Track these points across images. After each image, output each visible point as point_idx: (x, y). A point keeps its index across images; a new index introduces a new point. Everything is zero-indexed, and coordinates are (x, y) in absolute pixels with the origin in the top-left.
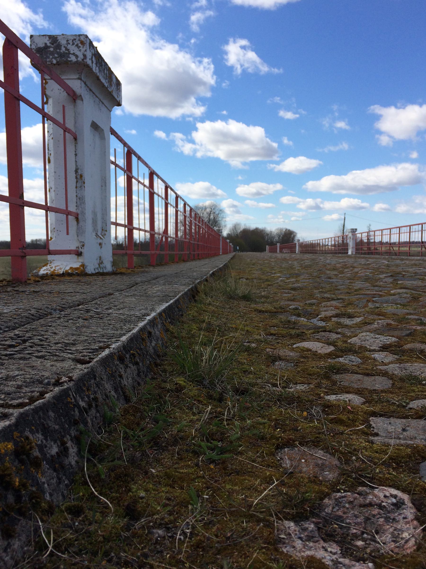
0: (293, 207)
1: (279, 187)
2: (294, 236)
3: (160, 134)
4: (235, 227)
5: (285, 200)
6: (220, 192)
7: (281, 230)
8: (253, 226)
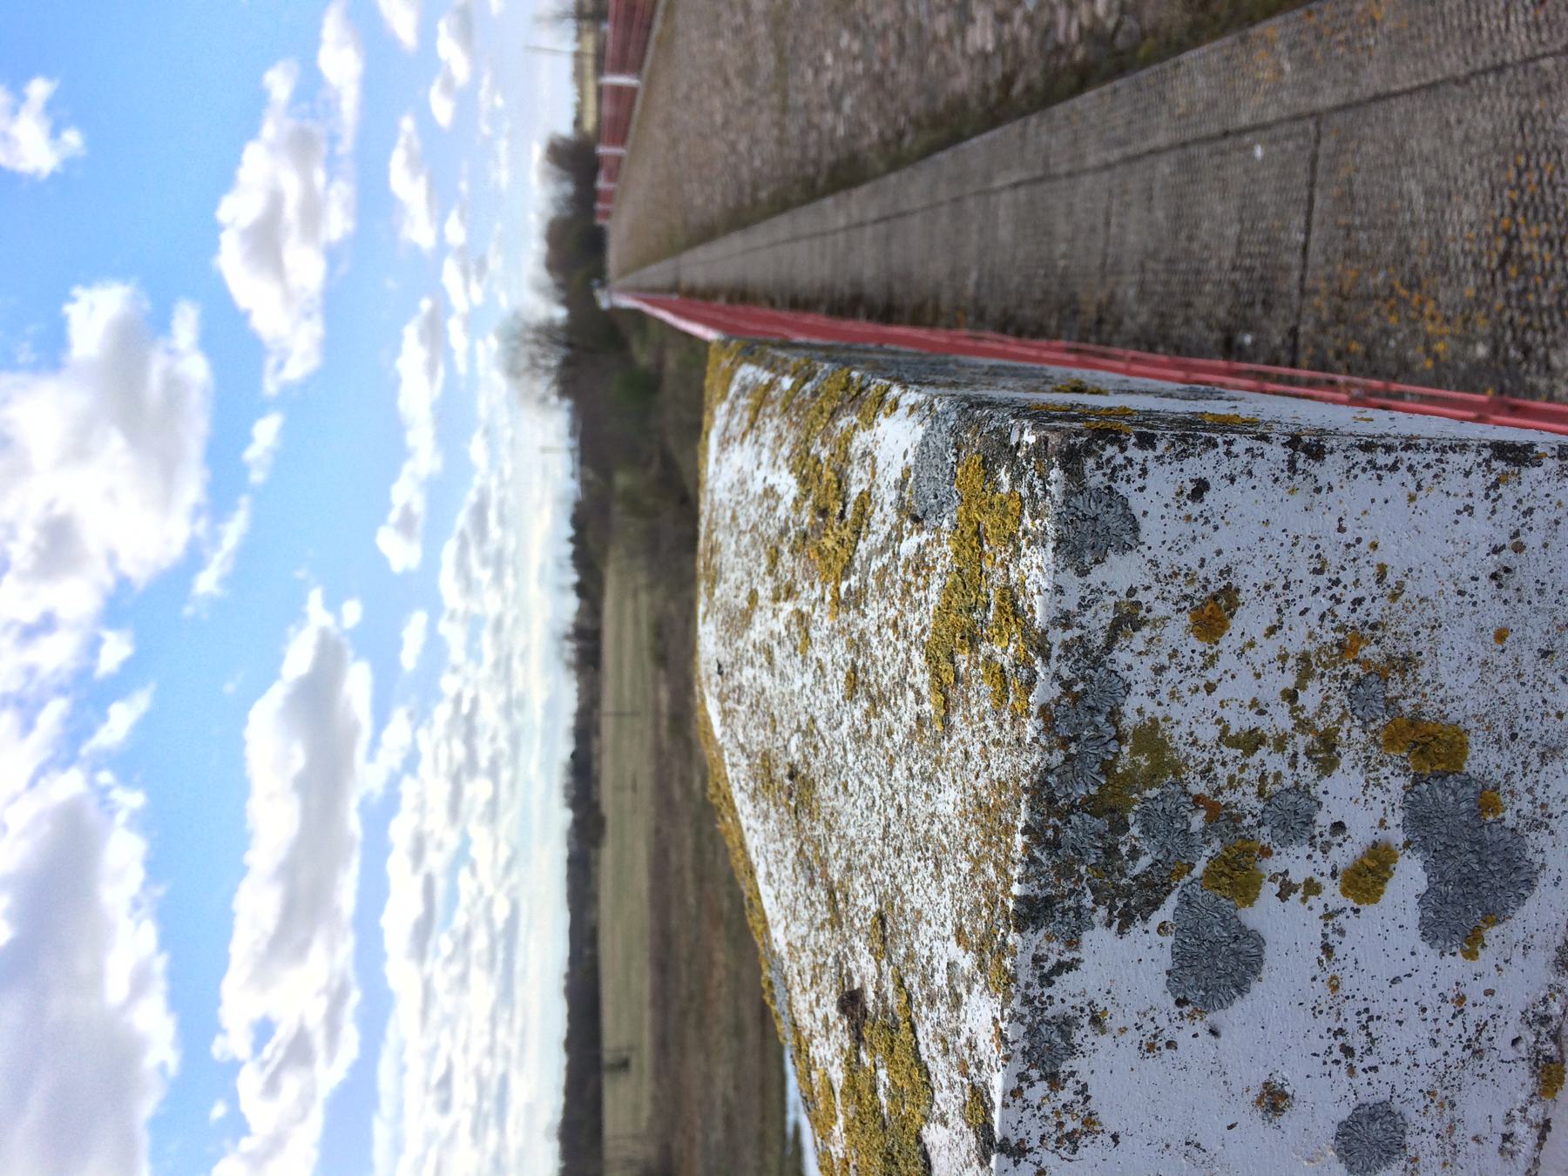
0: (465, 101)
1: (407, 124)
3: (266, 431)
4: (540, 289)
5: (442, 110)
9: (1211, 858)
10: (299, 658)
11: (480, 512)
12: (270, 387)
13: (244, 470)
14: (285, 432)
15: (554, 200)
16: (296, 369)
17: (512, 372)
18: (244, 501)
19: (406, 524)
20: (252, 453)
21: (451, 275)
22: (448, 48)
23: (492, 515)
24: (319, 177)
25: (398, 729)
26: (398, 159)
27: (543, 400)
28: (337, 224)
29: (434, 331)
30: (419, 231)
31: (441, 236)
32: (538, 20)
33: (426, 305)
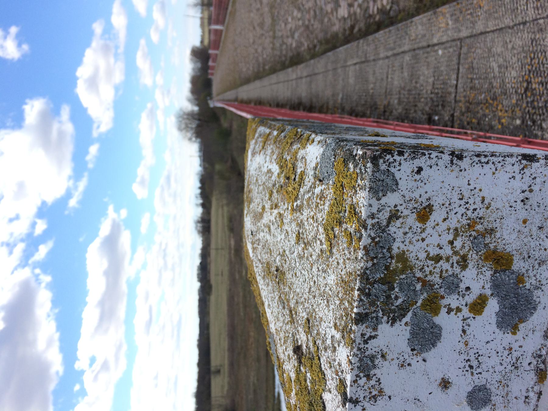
1: (143, 42)
2: (197, 48)
3: (93, 149)
4: (189, 100)
5: (155, 37)
6: (149, 105)
7: (191, 60)
8: (187, 86)
9: (423, 299)
10: (105, 229)
11: (168, 178)
12: (95, 134)
13: (86, 163)
14: (100, 150)
15: (194, 69)
16: (104, 128)
17: (180, 129)
18: (86, 174)
19: (143, 182)
20: (88, 158)
21: (158, 95)
22: (157, 15)
23: (172, 179)
24: (112, 60)
25: (140, 249)
26: (139, 54)
27: (190, 139)
28: (118, 77)
29: (152, 114)
30: (147, 80)
31: (154, 82)
32: (188, 5)
33: (149, 105)
